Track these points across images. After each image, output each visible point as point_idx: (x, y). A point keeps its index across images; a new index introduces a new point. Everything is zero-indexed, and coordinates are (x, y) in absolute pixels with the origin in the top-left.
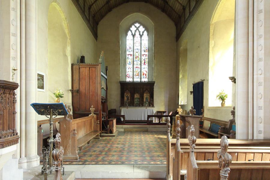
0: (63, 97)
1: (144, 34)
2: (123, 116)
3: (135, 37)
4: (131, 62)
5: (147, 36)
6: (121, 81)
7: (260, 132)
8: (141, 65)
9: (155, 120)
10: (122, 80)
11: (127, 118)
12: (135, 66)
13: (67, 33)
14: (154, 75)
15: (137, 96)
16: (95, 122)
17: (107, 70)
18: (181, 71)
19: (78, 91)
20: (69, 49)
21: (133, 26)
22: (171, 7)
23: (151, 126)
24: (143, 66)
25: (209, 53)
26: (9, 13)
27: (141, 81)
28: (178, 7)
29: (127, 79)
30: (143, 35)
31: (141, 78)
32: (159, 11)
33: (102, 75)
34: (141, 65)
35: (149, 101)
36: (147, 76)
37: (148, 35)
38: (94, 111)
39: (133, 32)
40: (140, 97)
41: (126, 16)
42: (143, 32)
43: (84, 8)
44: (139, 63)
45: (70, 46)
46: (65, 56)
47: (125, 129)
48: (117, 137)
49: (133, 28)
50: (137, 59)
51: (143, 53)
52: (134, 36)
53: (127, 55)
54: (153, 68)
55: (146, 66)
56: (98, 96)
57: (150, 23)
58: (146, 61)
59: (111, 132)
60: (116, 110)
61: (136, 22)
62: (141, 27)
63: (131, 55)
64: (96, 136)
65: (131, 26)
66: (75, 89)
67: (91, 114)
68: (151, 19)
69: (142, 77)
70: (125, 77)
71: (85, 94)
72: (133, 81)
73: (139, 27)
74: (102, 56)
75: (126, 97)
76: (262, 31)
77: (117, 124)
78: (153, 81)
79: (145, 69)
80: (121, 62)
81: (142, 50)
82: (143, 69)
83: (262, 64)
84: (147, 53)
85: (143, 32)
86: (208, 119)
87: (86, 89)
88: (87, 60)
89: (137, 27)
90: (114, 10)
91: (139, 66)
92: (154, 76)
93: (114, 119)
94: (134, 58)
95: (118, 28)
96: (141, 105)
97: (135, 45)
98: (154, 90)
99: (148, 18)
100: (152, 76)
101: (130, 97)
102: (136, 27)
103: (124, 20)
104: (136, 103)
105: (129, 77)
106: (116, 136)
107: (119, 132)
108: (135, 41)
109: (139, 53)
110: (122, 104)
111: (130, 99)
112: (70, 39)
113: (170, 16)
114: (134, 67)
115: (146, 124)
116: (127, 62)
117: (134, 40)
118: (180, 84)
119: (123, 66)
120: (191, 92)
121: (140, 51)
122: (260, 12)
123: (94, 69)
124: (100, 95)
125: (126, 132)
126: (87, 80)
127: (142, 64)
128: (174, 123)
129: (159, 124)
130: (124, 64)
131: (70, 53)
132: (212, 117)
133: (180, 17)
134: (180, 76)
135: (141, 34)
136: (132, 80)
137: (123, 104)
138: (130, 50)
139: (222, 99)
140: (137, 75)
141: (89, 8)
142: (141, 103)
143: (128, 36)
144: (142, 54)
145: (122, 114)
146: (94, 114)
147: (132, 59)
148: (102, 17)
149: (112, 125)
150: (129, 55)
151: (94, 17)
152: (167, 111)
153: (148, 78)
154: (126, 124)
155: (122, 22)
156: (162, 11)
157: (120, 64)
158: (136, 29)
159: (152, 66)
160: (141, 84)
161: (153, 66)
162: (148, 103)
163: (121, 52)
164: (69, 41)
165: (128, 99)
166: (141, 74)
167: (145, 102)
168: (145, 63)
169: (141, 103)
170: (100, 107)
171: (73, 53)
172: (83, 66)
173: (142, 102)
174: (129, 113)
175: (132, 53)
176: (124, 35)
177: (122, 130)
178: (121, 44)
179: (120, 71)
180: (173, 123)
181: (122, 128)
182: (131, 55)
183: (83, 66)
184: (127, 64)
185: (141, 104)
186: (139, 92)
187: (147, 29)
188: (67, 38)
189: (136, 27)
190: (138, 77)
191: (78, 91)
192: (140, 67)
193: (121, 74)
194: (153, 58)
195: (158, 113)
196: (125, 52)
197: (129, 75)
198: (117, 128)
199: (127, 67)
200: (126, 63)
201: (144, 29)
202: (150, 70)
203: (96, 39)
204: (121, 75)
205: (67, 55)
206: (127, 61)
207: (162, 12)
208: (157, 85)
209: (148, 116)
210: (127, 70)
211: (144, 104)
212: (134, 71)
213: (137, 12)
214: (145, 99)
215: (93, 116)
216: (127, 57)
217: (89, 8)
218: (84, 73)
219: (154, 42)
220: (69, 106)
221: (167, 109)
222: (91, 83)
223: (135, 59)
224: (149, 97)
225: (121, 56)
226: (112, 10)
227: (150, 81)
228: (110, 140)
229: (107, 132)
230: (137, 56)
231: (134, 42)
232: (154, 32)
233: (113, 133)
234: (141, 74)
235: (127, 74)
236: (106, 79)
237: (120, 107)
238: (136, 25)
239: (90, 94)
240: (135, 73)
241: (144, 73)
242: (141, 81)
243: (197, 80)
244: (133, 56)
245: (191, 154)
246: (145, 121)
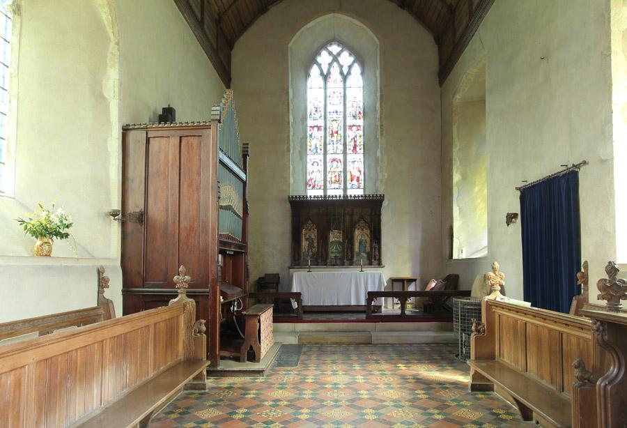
0: (67, 235)
1: (352, 71)
2: (298, 296)
3: (330, 80)
4: (318, 146)
5: (360, 78)
6: (296, 197)
8: (345, 153)
9: (390, 306)
10: (294, 194)
11: (308, 301)
12: (329, 157)
13: (106, 23)
14: (380, 177)
15: (335, 236)
16: (189, 328)
17: (245, 156)
18: (458, 163)
19: (142, 217)
20: (112, 78)
21: (324, 53)
23: (380, 325)
24: (350, 157)
25: (606, 56)
27: (345, 196)
29: (308, 191)
30: (350, 73)
31: (345, 189)
33: (221, 162)
34: (345, 153)
35: (368, 249)
36: (362, 182)
37: (362, 74)
38: (187, 286)
39: (319, 71)
40: (343, 241)
41: (306, 24)
42: (350, 67)
43: (202, 14)
44: (341, 147)
45: (117, 67)
47: (301, 335)
48: (274, 371)
49: (324, 58)
50: (335, 139)
51: (350, 121)
52: (326, 77)
53: (309, 129)
54: (377, 159)
55: (360, 156)
56: (207, 234)
57: (367, 37)
58: (358, 143)
59: (253, 356)
60: (280, 276)
61: (330, 42)
62: (345, 54)
63: (319, 128)
64: (195, 379)
65: (318, 53)
67: (175, 298)
69: (349, 186)
70: (303, 187)
71: (166, 228)
72: (325, 196)
73: (339, 54)
74: (225, 104)
75: (307, 240)
78: (379, 193)
79: (357, 163)
80: (294, 145)
81: (348, 113)
82: (352, 165)
84: (360, 122)
85: (350, 67)
87: (167, 210)
88: (182, 117)
89: (335, 53)
91: (341, 157)
92: (381, 180)
93: (263, 311)
94: (328, 135)
95: (284, 55)
96: (345, 261)
97: (328, 102)
98: (382, 218)
99: (363, 25)
100: (376, 180)
101: (315, 241)
102: (330, 53)
103: (298, 34)
104: (332, 256)
105: (314, 187)
106: (265, 374)
107: (283, 345)
108: (329, 91)
109: (338, 122)
110: (295, 260)
111: (316, 245)
112: (118, 44)
114: (328, 160)
115: (363, 316)
116: (309, 148)
117: (325, 88)
118: (454, 199)
119: (299, 157)
120: (510, 218)
121: (342, 116)
123: (194, 141)
124: (213, 230)
127: (348, 152)
128: (476, 327)
129: (401, 318)
130: (300, 153)
131: (117, 90)
134: (454, 177)
135: (345, 71)
136: (322, 194)
137: (297, 260)
138: (317, 115)
140: (336, 181)
142: (347, 256)
143: (310, 79)
144: (348, 124)
145: (295, 289)
146: (189, 296)
147: (323, 138)
149: (254, 333)
150: (313, 127)
151: (218, 22)
153: (364, 189)
154: (306, 317)
155: (294, 39)
156: (399, 6)
157: (289, 151)
158: (331, 58)
159: (376, 153)
160: (346, 204)
161: (379, 154)
162: (365, 255)
163: (294, 117)
164: (112, 47)
165: (311, 246)
166: (344, 177)
167: (359, 254)
168: (355, 147)
169: (347, 256)
171: (127, 92)
172: (159, 134)
173: (349, 254)
175: (321, 123)
176: (302, 74)
177: (293, 340)
178: (293, 97)
179: (291, 169)
180: (473, 328)
181: (293, 332)
182: (319, 128)
183: (159, 134)
184: (309, 152)
185: (347, 260)
186: (342, 227)
187: (360, 58)
189: (330, 53)
190: (337, 185)
191: (142, 217)
192: (342, 161)
193: (294, 177)
194: (379, 132)
195: (394, 283)
196: (305, 119)
197: (313, 181)
198: (275, 331)
199: (308, 160)
200: (306, 149)
201: (352, 59)
202: (369, 171)
204: (292, 181)
205: (105, 95)
206: (308, 144)
207: (399, 9)
208: (388, 204)
209: (370, 293)
210: (310, 168)
211: (355, 259)
212: (328, 169)
213: (334, 11)
215: (185, 306)
216: (309, 133)
218: (162, 156)
219: (379, 89)
220: (102, 267)
221: (418, 270)
223: (329, 138)
224: (368, 240)
225: (291, 130)
226: (268, 10)
227: (371, 193)
228: (245, 389)
229: (238, 355)
230: (335, 130)
231: (325, 93)
232: (378, 61)
233: (258, 361)
234: (344, 177)
235: (308, 178)
236: (244, 183)
237: (290, 268)
238: (330, 48)
239: (182, 226)
240: (329, 176)
241: (353, 174)
242: (345, 196)
243: (536, 173)
244: (325, 129)
246: (362, 309)
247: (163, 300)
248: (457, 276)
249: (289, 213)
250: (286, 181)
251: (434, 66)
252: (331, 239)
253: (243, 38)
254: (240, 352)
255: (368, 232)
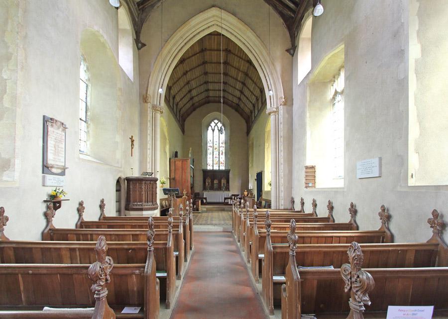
2: (206, 198)
7: (282, 205)
11: (208, 201)
12: (214, 156)
15: (216, 182)
20: (168, 147)
21: (213, 122)
22: (242, 109)
24: (221, 156)
26: (147, 137)
28: (247, 110)
31: (219, 167)
32: (234, 111)
43: (169, 98)
46: (165, 152)
47: (207, 208)
49: (213, 124)
51: (221, 145)
52: (213, 130)
61: (215, 119)
62: (219, 123)
66: (172, 177)
68: (227, 117)
76: (282, 149)
77: (201, 204)
79: (223, 158)
83: (282, 166)
84: (224, 145)
86: (264, 200)
90: (198, 110)
113: (241, 115)
122: (281, 137)
125: (208, 211)
126: (181, 170)
132: (266, 199)
133: (249, 117)
137: (205, 189)
139: (102, 207)
141: (180, 111)
145: (205, 197)
148: (188, 115)
152: (240, 194)
158: (215, 124)
160: (219, 171)
164: (168, 141)
165: (209, 184)
170: (190, 190)
174: (210, 195)
177: (205, 209)
188: (166, 139)
191: (174, 179)
203: (184, 134)
213: (216, 111)
214: (222, 185)
217: (180, 111)
222: (183, 174)
238: (215, 121)
243: (259, 171)
245: (267, 238)
247: (181, 197)
248: (65, 175)
249: (202, 174)
250: (201, 164)
251: (246, 131)
252: (215, 182)
253: (188, 118)
254: (167, 240)
255: (225, 180)
